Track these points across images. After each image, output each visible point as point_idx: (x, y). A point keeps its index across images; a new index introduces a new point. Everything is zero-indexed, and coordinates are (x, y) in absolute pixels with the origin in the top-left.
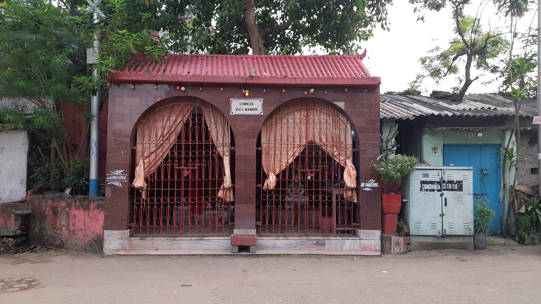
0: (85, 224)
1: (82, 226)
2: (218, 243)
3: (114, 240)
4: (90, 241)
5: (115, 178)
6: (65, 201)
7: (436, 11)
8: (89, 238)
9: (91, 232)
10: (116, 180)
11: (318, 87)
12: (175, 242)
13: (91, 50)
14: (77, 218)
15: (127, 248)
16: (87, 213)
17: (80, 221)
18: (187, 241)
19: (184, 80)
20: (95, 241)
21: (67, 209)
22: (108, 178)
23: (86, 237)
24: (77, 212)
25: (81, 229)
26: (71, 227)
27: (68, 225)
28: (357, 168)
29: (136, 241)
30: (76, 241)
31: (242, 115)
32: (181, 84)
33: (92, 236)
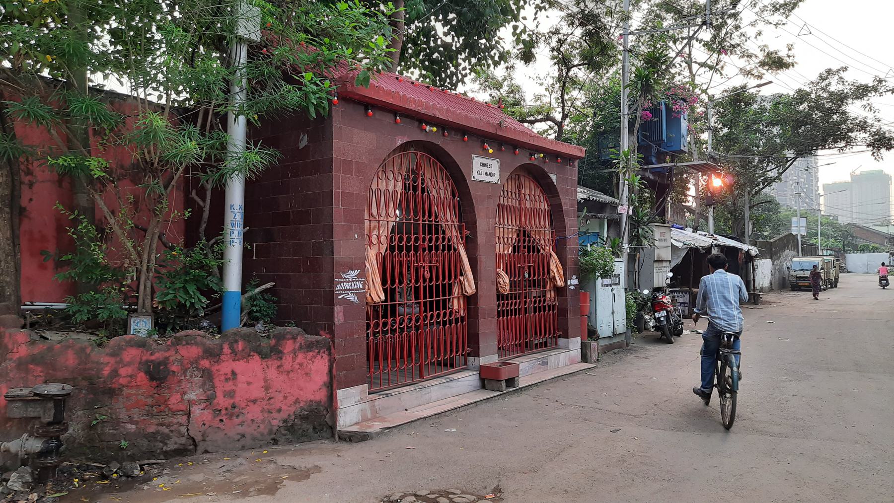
2: (461, 386)
3: (352, 407)
4: (285, 421)
5: (347, 286)
6: (196, 344)
8: (283, 415)
9: (291, 399)
10: (349, 290)
11: (444, 126)
12: (424, 391)
13: (840, 218)
16: (273, 363)
17: (249, 384)
18: (435, 387)
20: (304, 418)
22: (338, 287)
23: (275, 415)
25: (254, 401)
26: (222, 401)
27: (209, 399)
28: (563, 264)
29: (380, 402)
31: (482, 181)
32: (540, 150)
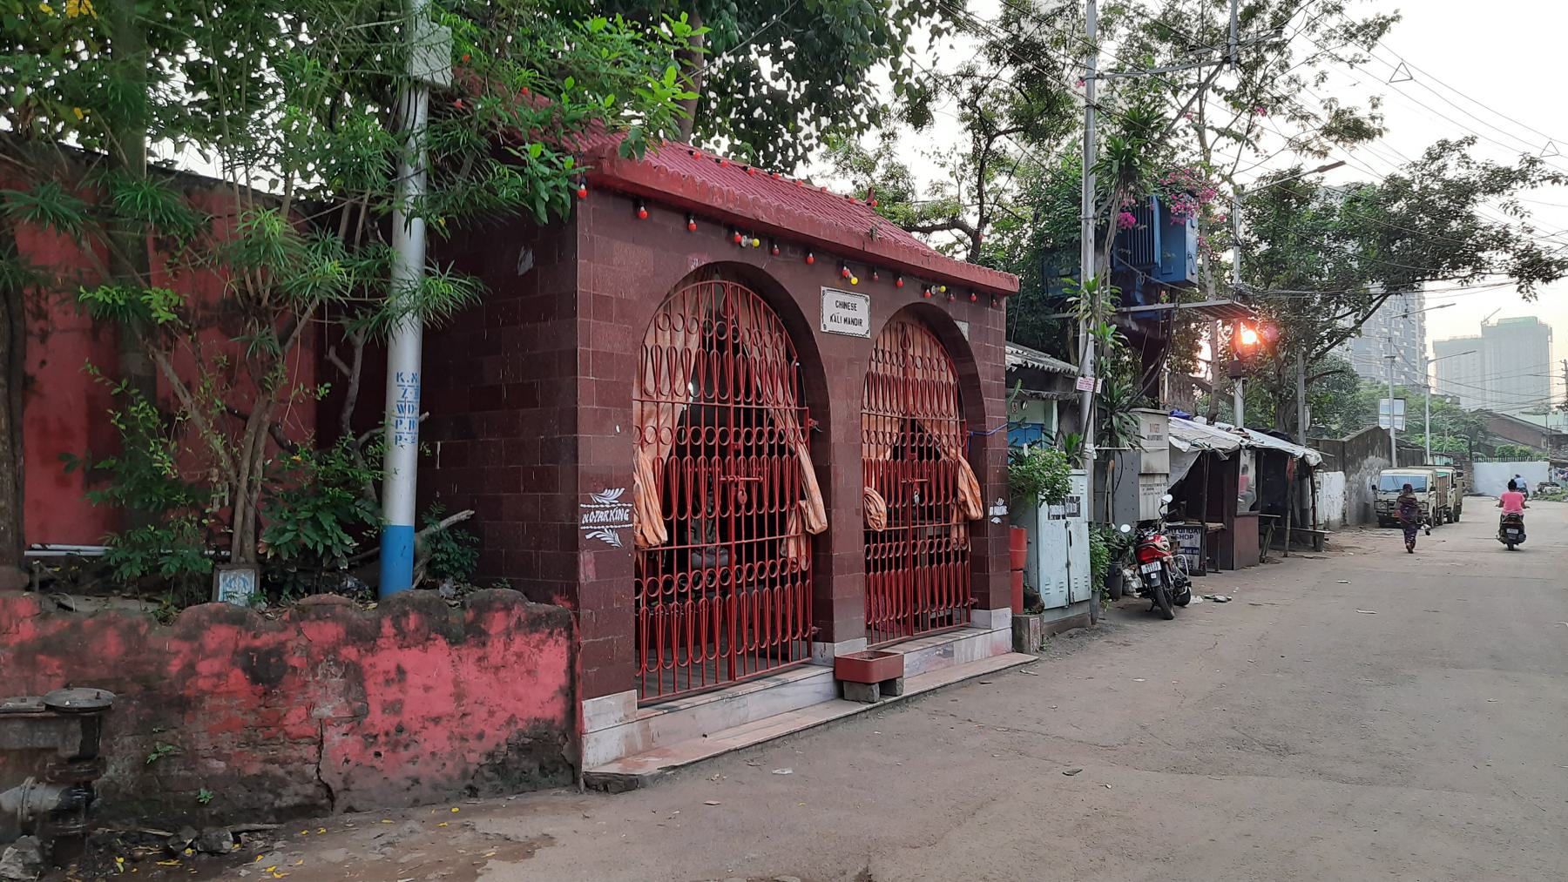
0: (459, 697)
1: (443, 705)
3: (609, 730)
4: (490, 755)
5: (602, 516)
6: (335, 618)
7: (911, 126)
8: (487, 744)
9: (501, 717)
10: (605, 524)
12: (735, 704)
14: (412, 679)
15: (640, 747)
16: (470, 653)
17: (427, 689)
18: (757, 696)
19: (736, 210)
21: (350, 653)
23: (473, 744)
24: (410, 658)
25: (437, 720)
26: (379, 720)
28: (981, 478)
29: (660, 721)
30: (412, 770)
31: (839, 334)
33: (504, 734)
